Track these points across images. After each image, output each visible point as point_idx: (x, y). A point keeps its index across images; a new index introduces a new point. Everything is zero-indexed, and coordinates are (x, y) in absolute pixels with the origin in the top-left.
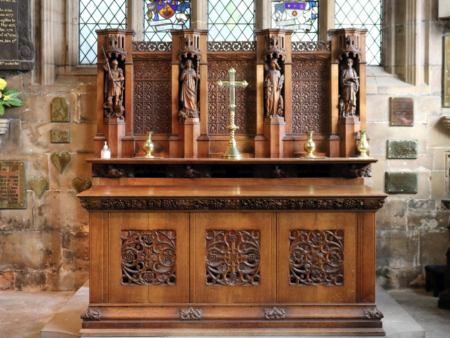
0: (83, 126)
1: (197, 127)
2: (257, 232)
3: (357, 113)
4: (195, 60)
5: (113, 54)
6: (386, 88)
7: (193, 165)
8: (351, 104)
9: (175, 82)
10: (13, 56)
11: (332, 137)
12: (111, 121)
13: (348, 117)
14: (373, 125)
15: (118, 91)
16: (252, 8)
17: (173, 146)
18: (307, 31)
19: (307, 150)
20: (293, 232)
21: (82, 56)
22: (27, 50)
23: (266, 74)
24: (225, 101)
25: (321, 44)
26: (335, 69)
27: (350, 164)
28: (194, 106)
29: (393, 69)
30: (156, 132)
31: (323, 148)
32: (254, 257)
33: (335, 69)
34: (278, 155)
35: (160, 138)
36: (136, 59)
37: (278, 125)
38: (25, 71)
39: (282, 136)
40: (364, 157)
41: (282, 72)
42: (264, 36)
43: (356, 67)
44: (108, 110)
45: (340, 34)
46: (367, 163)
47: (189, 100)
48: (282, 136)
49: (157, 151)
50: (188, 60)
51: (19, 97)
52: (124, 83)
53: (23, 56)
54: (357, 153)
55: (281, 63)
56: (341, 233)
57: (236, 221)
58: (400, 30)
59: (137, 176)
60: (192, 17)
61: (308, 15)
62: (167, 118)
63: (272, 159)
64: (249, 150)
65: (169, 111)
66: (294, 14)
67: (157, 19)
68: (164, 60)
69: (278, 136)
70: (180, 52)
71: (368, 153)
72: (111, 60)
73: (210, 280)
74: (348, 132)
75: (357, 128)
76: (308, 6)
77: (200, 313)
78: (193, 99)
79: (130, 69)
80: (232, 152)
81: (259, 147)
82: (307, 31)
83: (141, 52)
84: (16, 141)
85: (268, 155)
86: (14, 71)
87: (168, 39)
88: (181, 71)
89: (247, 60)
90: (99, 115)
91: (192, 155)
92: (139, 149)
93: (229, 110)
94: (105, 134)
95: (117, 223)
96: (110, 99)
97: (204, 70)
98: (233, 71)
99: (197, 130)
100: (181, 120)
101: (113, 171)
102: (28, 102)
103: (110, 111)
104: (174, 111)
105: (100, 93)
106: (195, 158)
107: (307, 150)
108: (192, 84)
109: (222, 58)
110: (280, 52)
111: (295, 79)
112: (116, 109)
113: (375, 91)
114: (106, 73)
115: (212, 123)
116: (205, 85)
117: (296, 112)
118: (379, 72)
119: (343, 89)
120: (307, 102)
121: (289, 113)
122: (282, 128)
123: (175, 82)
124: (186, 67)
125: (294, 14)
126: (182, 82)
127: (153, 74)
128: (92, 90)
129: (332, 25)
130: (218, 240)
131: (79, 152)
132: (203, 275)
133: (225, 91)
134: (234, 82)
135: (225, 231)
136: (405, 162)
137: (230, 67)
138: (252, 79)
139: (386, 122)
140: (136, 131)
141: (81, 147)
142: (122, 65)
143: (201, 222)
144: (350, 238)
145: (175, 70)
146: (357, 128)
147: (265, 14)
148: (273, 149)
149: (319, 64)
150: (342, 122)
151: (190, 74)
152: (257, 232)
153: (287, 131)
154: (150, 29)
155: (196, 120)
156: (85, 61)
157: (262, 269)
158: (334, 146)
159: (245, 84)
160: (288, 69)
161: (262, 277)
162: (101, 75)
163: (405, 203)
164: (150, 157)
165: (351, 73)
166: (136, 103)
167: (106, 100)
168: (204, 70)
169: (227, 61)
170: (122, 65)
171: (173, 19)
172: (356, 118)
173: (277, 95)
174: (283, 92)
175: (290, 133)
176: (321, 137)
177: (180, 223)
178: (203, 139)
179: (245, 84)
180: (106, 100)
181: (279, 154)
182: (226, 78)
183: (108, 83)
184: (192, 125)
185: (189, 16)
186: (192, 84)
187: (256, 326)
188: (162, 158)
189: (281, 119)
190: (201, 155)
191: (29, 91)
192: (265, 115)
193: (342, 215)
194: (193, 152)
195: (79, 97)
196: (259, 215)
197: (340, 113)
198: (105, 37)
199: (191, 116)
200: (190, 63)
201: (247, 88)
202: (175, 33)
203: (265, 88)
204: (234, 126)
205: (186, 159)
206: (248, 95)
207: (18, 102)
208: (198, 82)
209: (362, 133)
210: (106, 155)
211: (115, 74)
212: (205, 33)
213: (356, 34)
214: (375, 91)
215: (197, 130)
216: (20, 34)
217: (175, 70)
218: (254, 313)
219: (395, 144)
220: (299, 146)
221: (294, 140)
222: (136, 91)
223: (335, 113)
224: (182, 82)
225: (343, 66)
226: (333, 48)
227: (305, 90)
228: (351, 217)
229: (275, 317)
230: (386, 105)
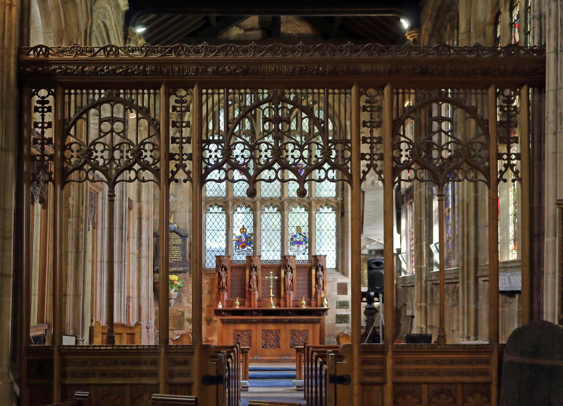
0: (209, 295)
1: (257, 295)
2: (279, 331)
3: (323, 289)
4: (256, 268)
5: (223, 266)
6: (336, 279)
7: (256, 311)
8: (320, 286)
9: (247, 277)
10: (180, 266)
11: (312, 299)
12: (221, 293)
13: (318, 291)
14: (330, 294)
15: (224, 280)
16: (280, 244)
17: (247, 303)
18: (304, 254)
19: (302, 304)
20: (291, 330)
21: (206, 265)
22: (186, 264)
23: (285, 273)
24: (269, 284)
25: (309, 261)
26: (314, 271)
27: (319, 310)
28: (255, 286)
29: (340, 270)
30: (240, 297)
31: (309, 304)
32: (278, 340)
33: (314, 271)
34: (290, 307)
35: (241, 300)
36: (232, 268)
37: (290, 294)
38: (184, 272)
39: (292, 298)
40: (326, 307)
41: (292, 273)
42: (284, 258)
43: (322, 270)
44: (220, 288)
45: (315, 257)
46: (326, 310)
47: (253, 284)
48: (292, 298)
49: (240, 305)
50: (253, 268)
51: (182, 283)
52: (227, 278)
53: (184, 266)
54: (323, 306)
55: (291, 269)
56: (307, 331)
57: (272, 327)
58: (343, 254)
59: (232, 315)
60: (254, 248)
61: (304, 247)
62: (245, 292)
63: (288, 308)
64: (278, 304)
65: (245, 289)
66: (298, 246)
67: (239, 249)
68: (243, 268)
69: (290, 299)
70: (250, 264)
71: (327, 306)
72: (221, 268)
73: (263, 347)
74: (319, 297)
75: (323, 295)
76: (304, 243)
77: (260, 358)
78: (255, 284)
79: (229, 271)
80: (271, 305)
81: (282, 303)
82: (304, 254)
83: (233, 265)
84: (180, 301)
85: (286, 306)
86: (180, 272)
87: (244, 258)
88: (250, 272)
89: (278, 268)
90: (216, 290)
91: (255, 306)
92: (232, 304)
93: (270, 288)
94: (218, 299)
95: (232, 327)
96: (221, 284)
97: (260, 272)
98: (271, 272)
99: (257, 297)
100: (250, 292)
101: (223, 313)
102: (186, 285)
103: (221, 289)
104: (247, 289)
105: (216, 281)
106: (256, 308)
107: (302, 304)
108: (254, 277)
109: (268, 267)
110: (291, 265)
111: (297, 275)
112: (224, 288)
113: (331, 280)
114: (219, 273)
115: (263, 293)
116: (260, 278)
117: (298, 289)
118: (334, 271)
119: (317, 280)
120: (302, 284)
121: (295, 289)
122: (292, 296)
123: (247, 277)
124: (252, 271)
125: (298, 246)
126: (250, 277)
127: (238, 273)
128: (212, 280)
129: (313, 254)
130: (266, 333)
131: (207, 306)
132: (261, 345)
133: (269, 280)
134: (272, 277)
135: (268, 331)
136: (344, 310)
137: (270, 271)
138: (279, 275)
139: (336, 293)
140: (231, 297)
141: (208, 304)
142: (226, 270)
143: (260, 327)
144: (310, 333)
145: (248, 272)
146: (323, 295)
147: (285, 247)
148: (288, 304)
149: (307, 269)
150: (316, 293)
151: (254, 274)
152: (279, 331)
153: (294, 296)
154: (236, 253)
155: (256, 292)
156: (208, 267)
157: (281, 343)
158: (313, 303)
159: (276, 277)
160: (294, 271)
161: (281, 346)
162: (217, 274)
163: (344, 327)
164: (237, 307)
165: (320, 273)
166: (231, 285)
167: (219, 284)
168: (260, 272)
169: (269, 268)
170: (226, 270)
171: (246, 249)
172: (322, 292)
173: (290, 282)
174: (292, 281)
175: (296, 298)
176: (308, 299)
177: (253, 327)
178: (259, 300)
179: (276, 277)
180: (219, 284)
181: (291, 306)
182: (269, 275)
183: (220, 277)
184: (255, 294)
185: (253, 248)
186: (254, 277)
187: (278, 362)
188: (243, 308)
189: (291, 292)
190: (258, 306)
191: (186, 280)
192: (285, 290)
193: (307, 325)
194: (255, 306)
195: (207, 283)
196: (279, 325)
197: (316, 289)
198: (219, 259)
199: (254, 291)
200: (254, 269)
201: (277, 279)
202: (247, 257)
203: (285, 279)
204: (272, 295)
205: (252, 308)
206: (278, 282)
207: (182, 285)
208: (257, 277)
209: (324, 297)
210: (220, 307)
211: (223, 274)
212: (260, 256)
213: (322, 257)
214: (331, 280)
215: (257, 297)
216: (183, 257)
217: (248, 272)
218: (278, 358)
219: (340, 302)
220: (299, 303)
221: (296, 301)
222: (231, 280)
223: (314, 290)
224: (250, 277)
225: (317, 270)
226: (313, 263)
227: (302, 280)
228: (310, 326)
229: (285, 360)
230: (336, 286)
